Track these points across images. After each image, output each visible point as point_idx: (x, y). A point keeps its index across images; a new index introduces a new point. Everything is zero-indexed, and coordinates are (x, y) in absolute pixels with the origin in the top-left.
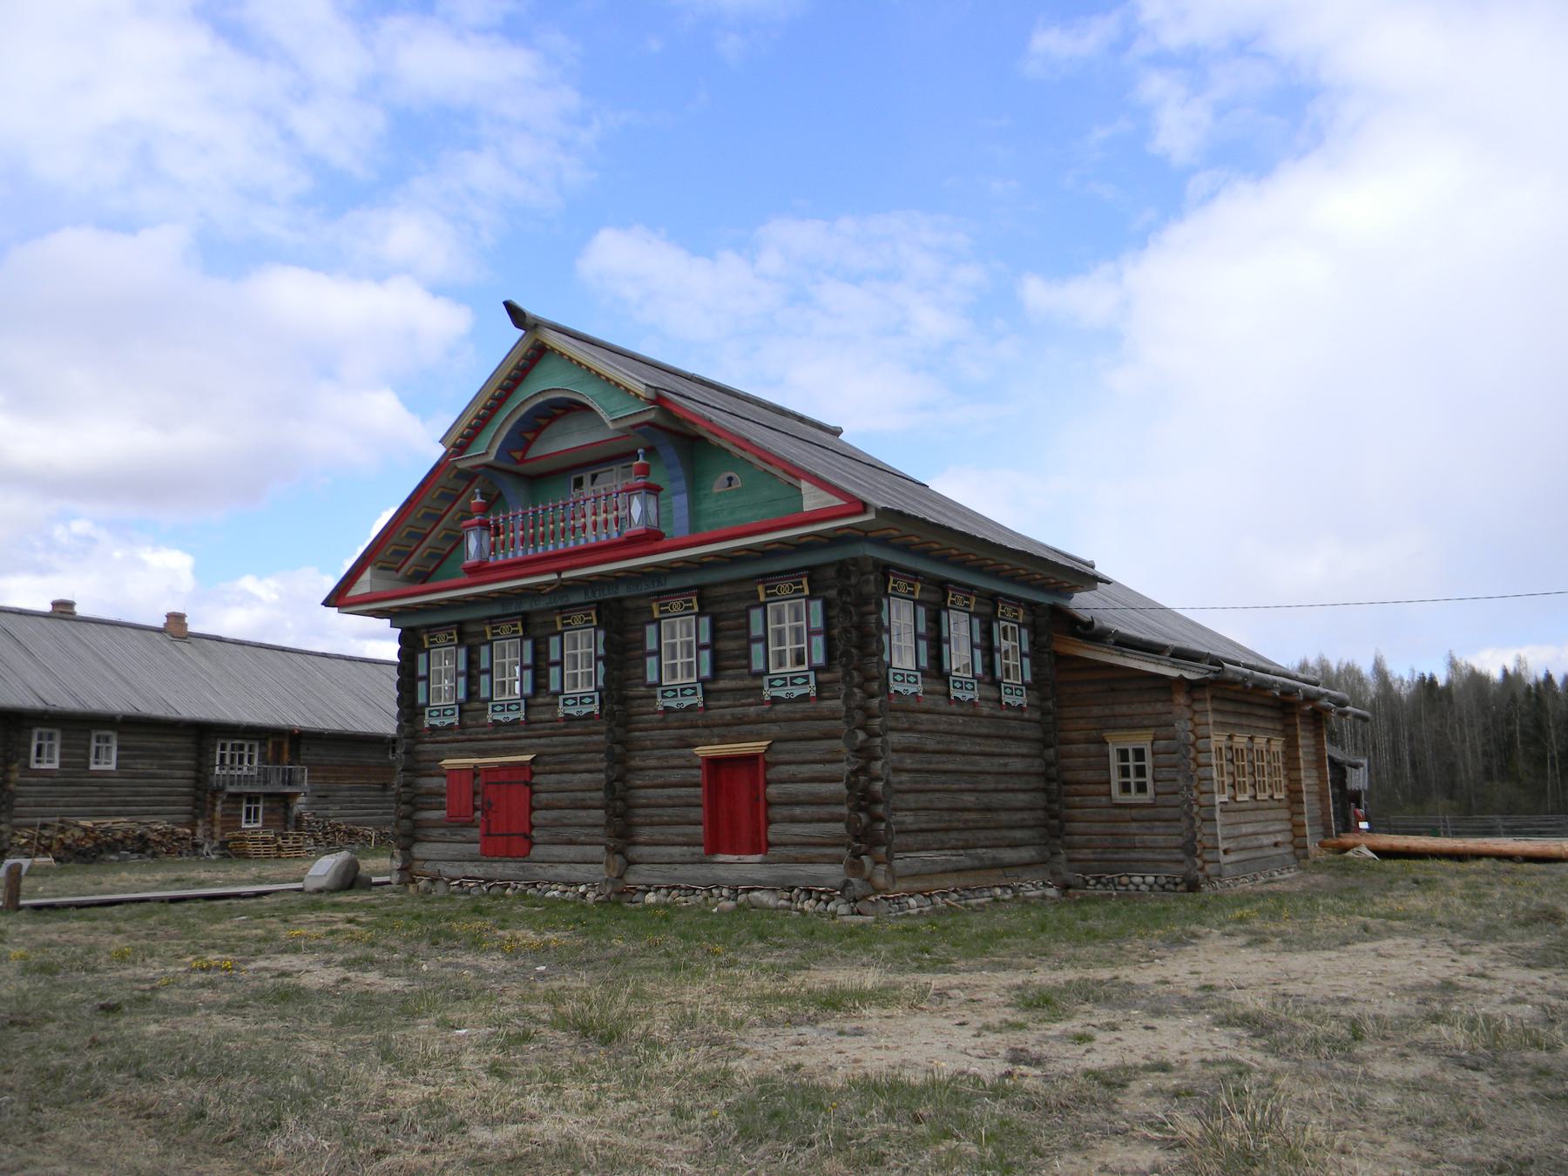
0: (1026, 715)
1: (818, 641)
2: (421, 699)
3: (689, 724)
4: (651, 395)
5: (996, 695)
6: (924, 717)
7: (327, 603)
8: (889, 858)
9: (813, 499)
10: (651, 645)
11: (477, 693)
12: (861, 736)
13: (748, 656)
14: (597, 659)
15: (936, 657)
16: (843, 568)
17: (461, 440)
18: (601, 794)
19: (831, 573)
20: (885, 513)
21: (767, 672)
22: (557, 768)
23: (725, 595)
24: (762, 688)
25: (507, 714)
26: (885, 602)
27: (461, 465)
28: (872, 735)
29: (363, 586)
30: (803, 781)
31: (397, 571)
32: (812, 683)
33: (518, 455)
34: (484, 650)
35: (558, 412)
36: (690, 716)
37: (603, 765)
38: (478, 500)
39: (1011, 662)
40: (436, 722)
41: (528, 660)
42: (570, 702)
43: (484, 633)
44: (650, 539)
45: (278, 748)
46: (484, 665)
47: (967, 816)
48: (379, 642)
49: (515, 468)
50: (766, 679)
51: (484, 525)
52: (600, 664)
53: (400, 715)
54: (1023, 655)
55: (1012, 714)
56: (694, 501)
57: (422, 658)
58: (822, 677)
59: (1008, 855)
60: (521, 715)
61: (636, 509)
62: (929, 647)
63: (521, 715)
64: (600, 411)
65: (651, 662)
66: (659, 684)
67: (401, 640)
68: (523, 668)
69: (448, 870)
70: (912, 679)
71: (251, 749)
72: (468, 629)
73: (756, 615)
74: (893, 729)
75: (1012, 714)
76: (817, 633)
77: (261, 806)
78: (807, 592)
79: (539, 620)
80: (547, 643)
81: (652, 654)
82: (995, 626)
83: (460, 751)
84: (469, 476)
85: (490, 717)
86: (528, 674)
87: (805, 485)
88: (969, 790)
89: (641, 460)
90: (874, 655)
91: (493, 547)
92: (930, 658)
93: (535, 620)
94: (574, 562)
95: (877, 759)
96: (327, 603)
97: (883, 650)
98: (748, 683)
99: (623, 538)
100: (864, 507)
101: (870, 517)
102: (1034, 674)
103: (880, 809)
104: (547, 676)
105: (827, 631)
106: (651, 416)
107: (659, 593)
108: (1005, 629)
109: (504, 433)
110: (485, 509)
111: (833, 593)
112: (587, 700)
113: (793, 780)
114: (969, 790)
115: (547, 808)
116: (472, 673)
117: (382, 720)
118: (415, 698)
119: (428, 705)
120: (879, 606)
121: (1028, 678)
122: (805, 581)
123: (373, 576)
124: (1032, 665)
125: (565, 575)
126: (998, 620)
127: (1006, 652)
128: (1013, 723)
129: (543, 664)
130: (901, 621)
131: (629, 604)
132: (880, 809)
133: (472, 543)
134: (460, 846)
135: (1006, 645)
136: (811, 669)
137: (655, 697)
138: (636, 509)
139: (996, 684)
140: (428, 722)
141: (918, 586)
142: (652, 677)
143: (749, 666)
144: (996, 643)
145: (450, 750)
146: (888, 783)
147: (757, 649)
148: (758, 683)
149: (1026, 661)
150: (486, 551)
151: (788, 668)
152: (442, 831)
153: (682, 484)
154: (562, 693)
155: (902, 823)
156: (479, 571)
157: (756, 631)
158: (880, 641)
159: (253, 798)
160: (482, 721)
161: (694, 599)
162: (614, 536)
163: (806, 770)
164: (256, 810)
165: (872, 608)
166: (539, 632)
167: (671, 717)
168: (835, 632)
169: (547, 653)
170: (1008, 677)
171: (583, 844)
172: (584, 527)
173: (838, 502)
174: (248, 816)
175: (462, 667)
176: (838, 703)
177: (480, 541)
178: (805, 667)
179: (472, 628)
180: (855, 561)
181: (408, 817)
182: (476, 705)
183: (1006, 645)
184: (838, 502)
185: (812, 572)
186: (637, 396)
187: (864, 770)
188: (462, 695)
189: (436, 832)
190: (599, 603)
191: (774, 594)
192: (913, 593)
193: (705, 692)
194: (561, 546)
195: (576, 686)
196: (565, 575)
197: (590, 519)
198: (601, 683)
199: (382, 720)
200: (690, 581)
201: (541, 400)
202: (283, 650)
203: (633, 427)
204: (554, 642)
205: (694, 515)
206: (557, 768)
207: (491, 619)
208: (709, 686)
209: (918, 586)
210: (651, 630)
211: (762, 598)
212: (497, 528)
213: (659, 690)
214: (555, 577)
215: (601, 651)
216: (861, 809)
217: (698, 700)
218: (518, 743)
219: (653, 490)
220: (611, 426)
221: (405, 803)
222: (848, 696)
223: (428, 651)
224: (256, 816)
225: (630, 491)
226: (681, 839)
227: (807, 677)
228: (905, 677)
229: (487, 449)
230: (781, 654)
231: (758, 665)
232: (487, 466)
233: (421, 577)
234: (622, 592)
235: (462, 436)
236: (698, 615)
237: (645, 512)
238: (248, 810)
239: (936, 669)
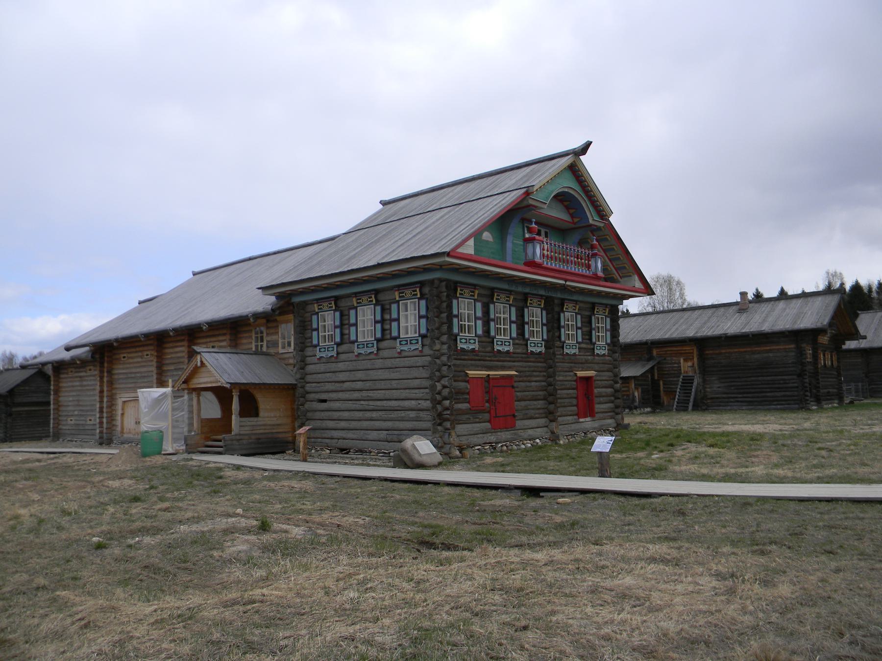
3: (574, 362)
22: (525, 379)
25: (409, 346)
36: (573, 358)
69: (474, 440)
76: (479, 319)
83: (477, 366)
94: (557, 275)
112: (414, 342)
125: (568, 283)
134: (478, 425)
141: (512, 297)
143: (312, 342)
145: (472, 365)
151: (409, 335)
152: (467, 416)
167: (566, 358)
171: (536, 418)
189: (464, 417)
195: (407, 333)
196: (568, 283)
202: (250, 259)
206: (525, 379)
209: (512, 297)
218: (506, 364)
226: (570, 413)
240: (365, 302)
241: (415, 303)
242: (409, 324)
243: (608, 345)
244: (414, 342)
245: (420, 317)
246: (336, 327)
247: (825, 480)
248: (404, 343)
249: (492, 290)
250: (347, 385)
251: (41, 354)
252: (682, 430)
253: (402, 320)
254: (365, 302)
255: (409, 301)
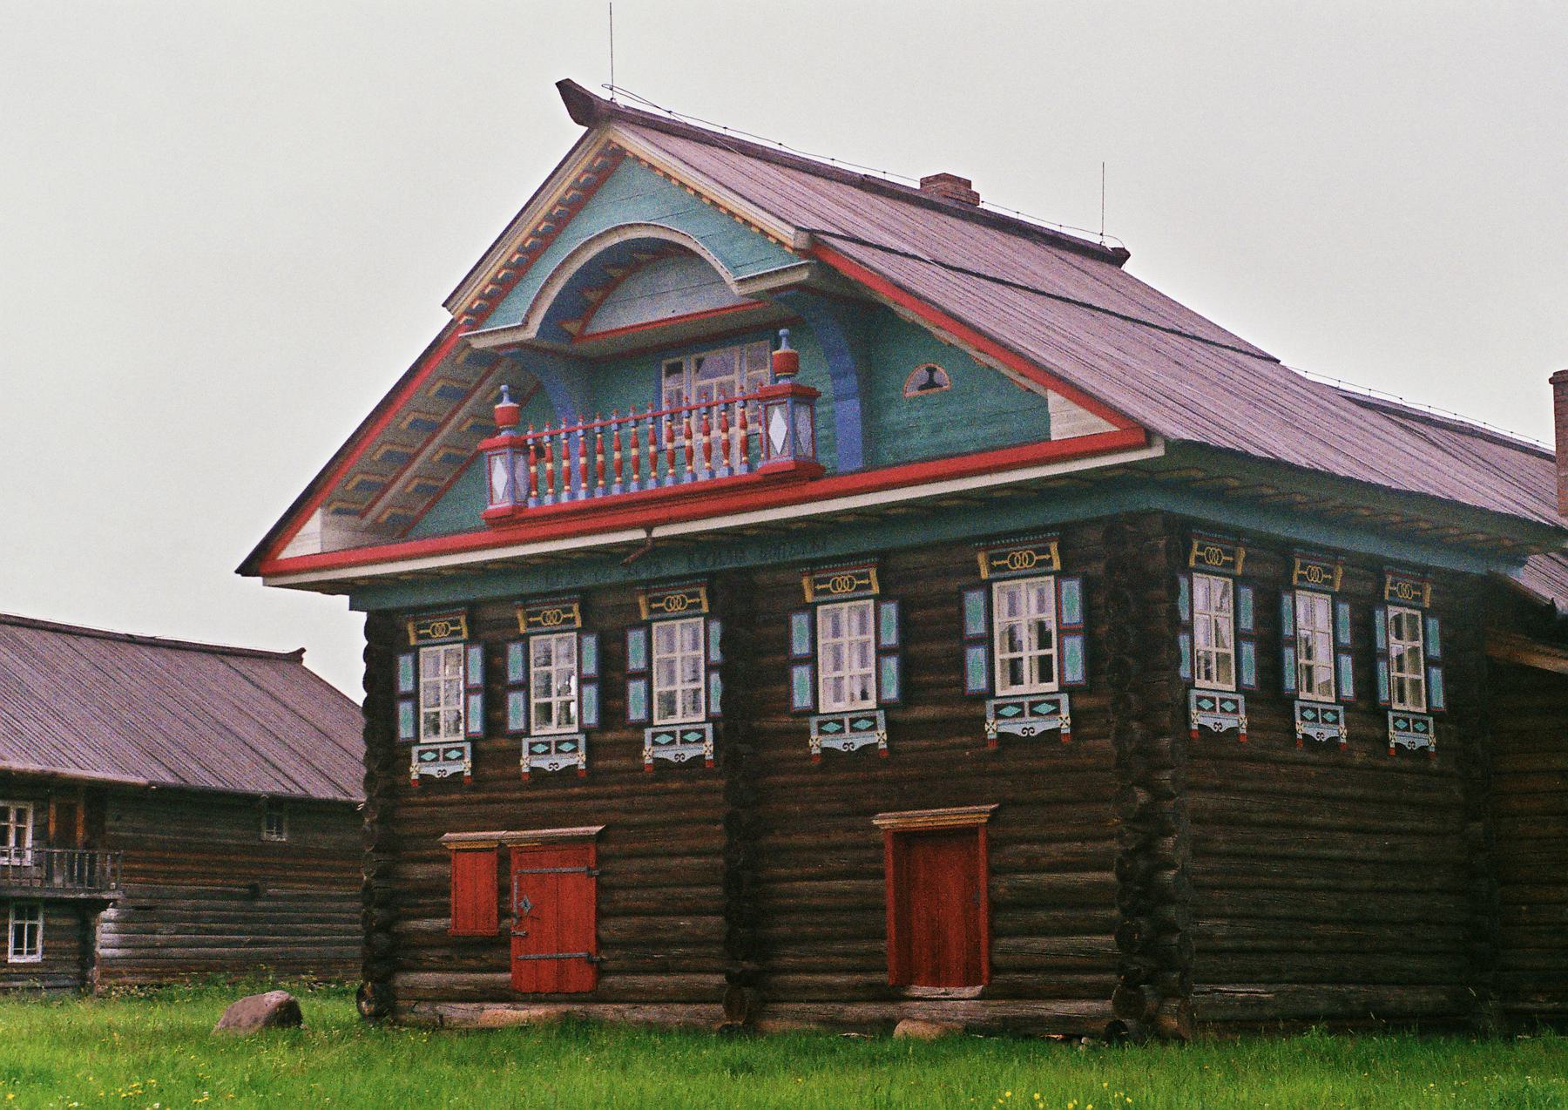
0: (1434, 765)
1: (1074, 645)
2: (405, 732)
4: (802, 241)
5: (1378, 733)
6: (1250, 767)
7: (245, 569)
8: (1182, 991)
9: (1066, 421)
10: (800, 647)
11: (504, 722)
12: (1142, 796)
13: (960, 665)
14: (710, 668)
15: (1271, 668)
16: (1113, 528)
17: (481, 299)
18: (718, 890)
19: (1094, 536)
20: (1179, 448)
21: (991, 693)
23: (927, 575)
24: (984, 719)
25: (555, 758)
26: (1184, 582)
27: (478, 344)
28: (1159, 794)
29: (311, 539)
30: (1053, 868)
31: (362, 515)
32: (1065, 713)
33: (573, 327)
34: (515, 651)
35: (644, 257)
37: (718, 842)
38: (506, 403)
39: (1408, 675)
40: (433, 771)
41: (590, 668)
42: (664, 739)
43: (514, 624)
44: (802, 476)
45: (67, 814)
46: (515, 675)
47: (1320, 929)
48: (334, 641)
49: (565, 347)
50: (990, 704)
51: (518, 447)
52: (715, 678)
53: (370, 757)
54: (1430, 662)
55: (1407, 763)
56: (871, 411)
57: (405, 662)
58: (1082, 702)
59: (1394, 996)
60: (579, 760)
61: (778, 429)
62: (1260, 653)
63: (579, 760)
64: (718, 265)
65: (800, 674)
66: (814, 711)
67: (368, 632)
68: (583, 681)
70: (1229, 706)
71: (21, 817)
72: (489, 616)
73: (974, 600)
74: (1191, 787)
75: (1407, 763)
77: (40, 923)
78: (1057, 566)
79: (611, 600)
80: (624, 642)
81: (801, 661)
82: (1379, 615)
84: (488, 360)
85: (526, 763)
86: (591, 692)
87: (1053, 398)
88: (1329, 889)
89: (784, 349)
90: (1167, 669)
91: (533, 483)
92: (1261, 670)
93: (609, 603)
95: (1170, 833)
96: (245, 569)
97: (1178, 661)
98: (958, 711)
99: (755, 477)
100: (1148, 436)
101: (1157, 452)
102: (1448, 696)
103: (1171, 912)
104: (624, 695)
105: (1088, 630)
106: (804, 275)
107: (814, 563)
108: (1398, 619)
109: (554, 292)
110: (515, 419)
111: (1097, 569)
112: (691, 737)
113: (1032, 866)
114: (1329, 889)
115: (627, 913)
116: (494, 688)
117: (339, 774)
118: (394, 732)
119: (417, 741)
120: (1174, 590)
121: (1439, 702)
122: (1054, 547)
123: (325, 524)
124: (1447, 680)
125: (658, 532)
126: (1384, 605)
127: (1400, 658)
128: (1408, 779)
129: (616, 675)
130: (1210, 610)
131: (764, 578)
132: (1171, 912)
133: (500, 477)
135: (1397, 647)
136: (1062, 689)
137: (807, 732)
138: (778, 429)
139: (1379, 713)
140: (416, 769)
142: (801, 700)
143: (962, 682)
144: (1381, 644)
146: (1183, 872)
147: (976, 655)
148: (977, 710)
149: (1436, 673)
150: (523, 489)
151: (678, 719)
153: (852, 382)
154: (650, 723)
155: (1209, 937)
156: (512, 523)
157: (975, 627)
158: (1175, 645)
159: (27, 908)
160: (510, 770)
161: (873, 573)
162: (740, 470)
163: (1055, 851)
164: (33, 929)
165: (1163, 593)
166: (609, 623)
168: (1103, 629)
169: (624, 657)
170: (1402, 700)
172: (690, 454)
173: (1106, 427)
174: (18, 943)
175: (476, 678)
176: (1107, 743)
177: (512, 470)
178: (1053, 686)
179: (492, 613)
180: (1136, 518)
181: (385, 927)
182: (504, 743)
183: (1397, 647)
184: (1106, 427)
185: (1066, 534)
186: (781, 243)
187: (1147, 848)
188: (476, 726)
190: (712, 576)
191: (1005, 568)
192: (1233, 565)
193: (891, 726)
194: (651, 485)
196: (658, 532)
197: (699, 439)
198: (716, 709)
199: (339, 774)
200: (865, 544)
201: (615, 240)
203: (772, 291)
204: (635, 638)
205: (873, 433)
207: (525, 599)
208: (899, 716)
210: (799, 622)
211: (984, 574)
212: (540, 452)
213: (814, 721)
214: (640, 535)
215: (716, 655)
216: (1140, 913)
217: (879, 737)
219: (804, 397)
220: (735, 289)
221: (380, 905)
222: (1121, 733)
223: (415, 651)
224: (32, 943)
225: (767, 399)
227: (1056, 703)
228: (1215, 704)
229: (521, 319)
230: (1015, 665)
231: (976, 682)
232: (523, 345)
233: (400, 530)
234: (751, 559)
235: (481, 296)
236: (879, 599)
237: (793, 434)
238: (19, 930)
239: (1271, 696)
240: (440, 635)
241: (863, 615)
242: (678, 687)
243: (1348, 706)
244: (454, 754)
245: (882, 652)
246: (469, 691)
247: (846, 995)
248: (540, 748)
249: (1376, 568)
250: (248, 938)
251: (1233, 1075)
252: (194, 981)
253: (824, 658)
254: (843, 590)
255: (678, 623)
